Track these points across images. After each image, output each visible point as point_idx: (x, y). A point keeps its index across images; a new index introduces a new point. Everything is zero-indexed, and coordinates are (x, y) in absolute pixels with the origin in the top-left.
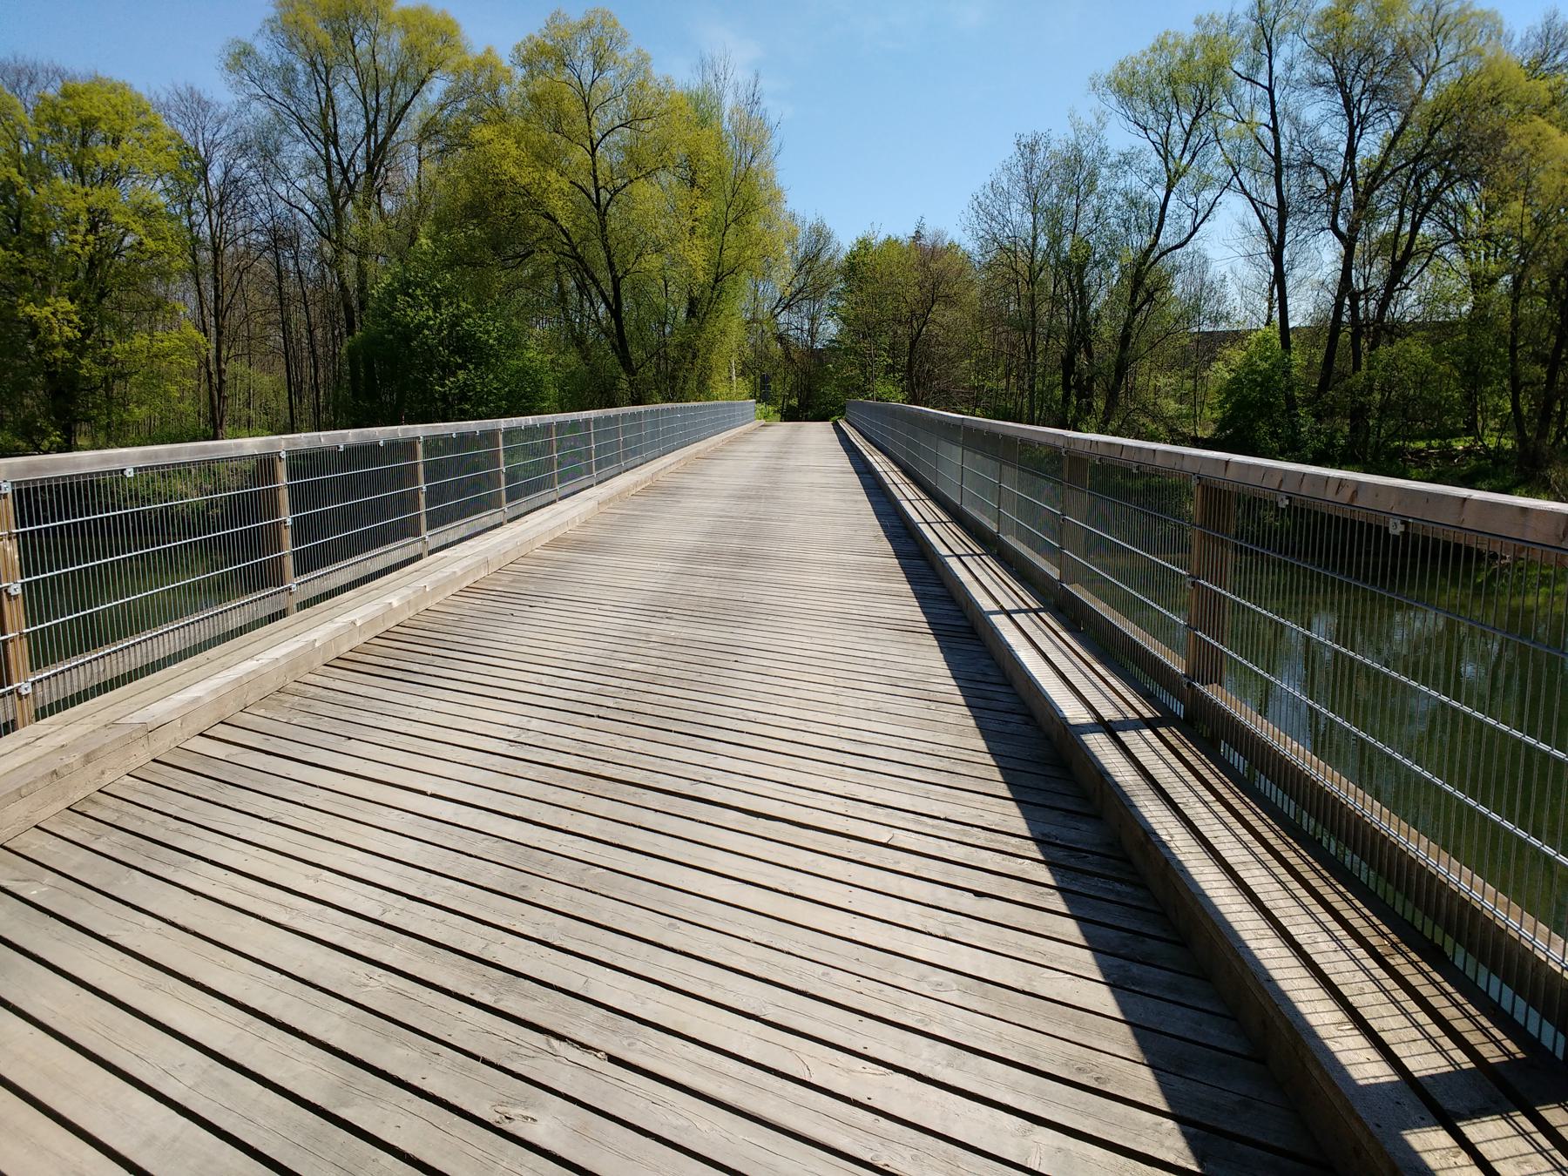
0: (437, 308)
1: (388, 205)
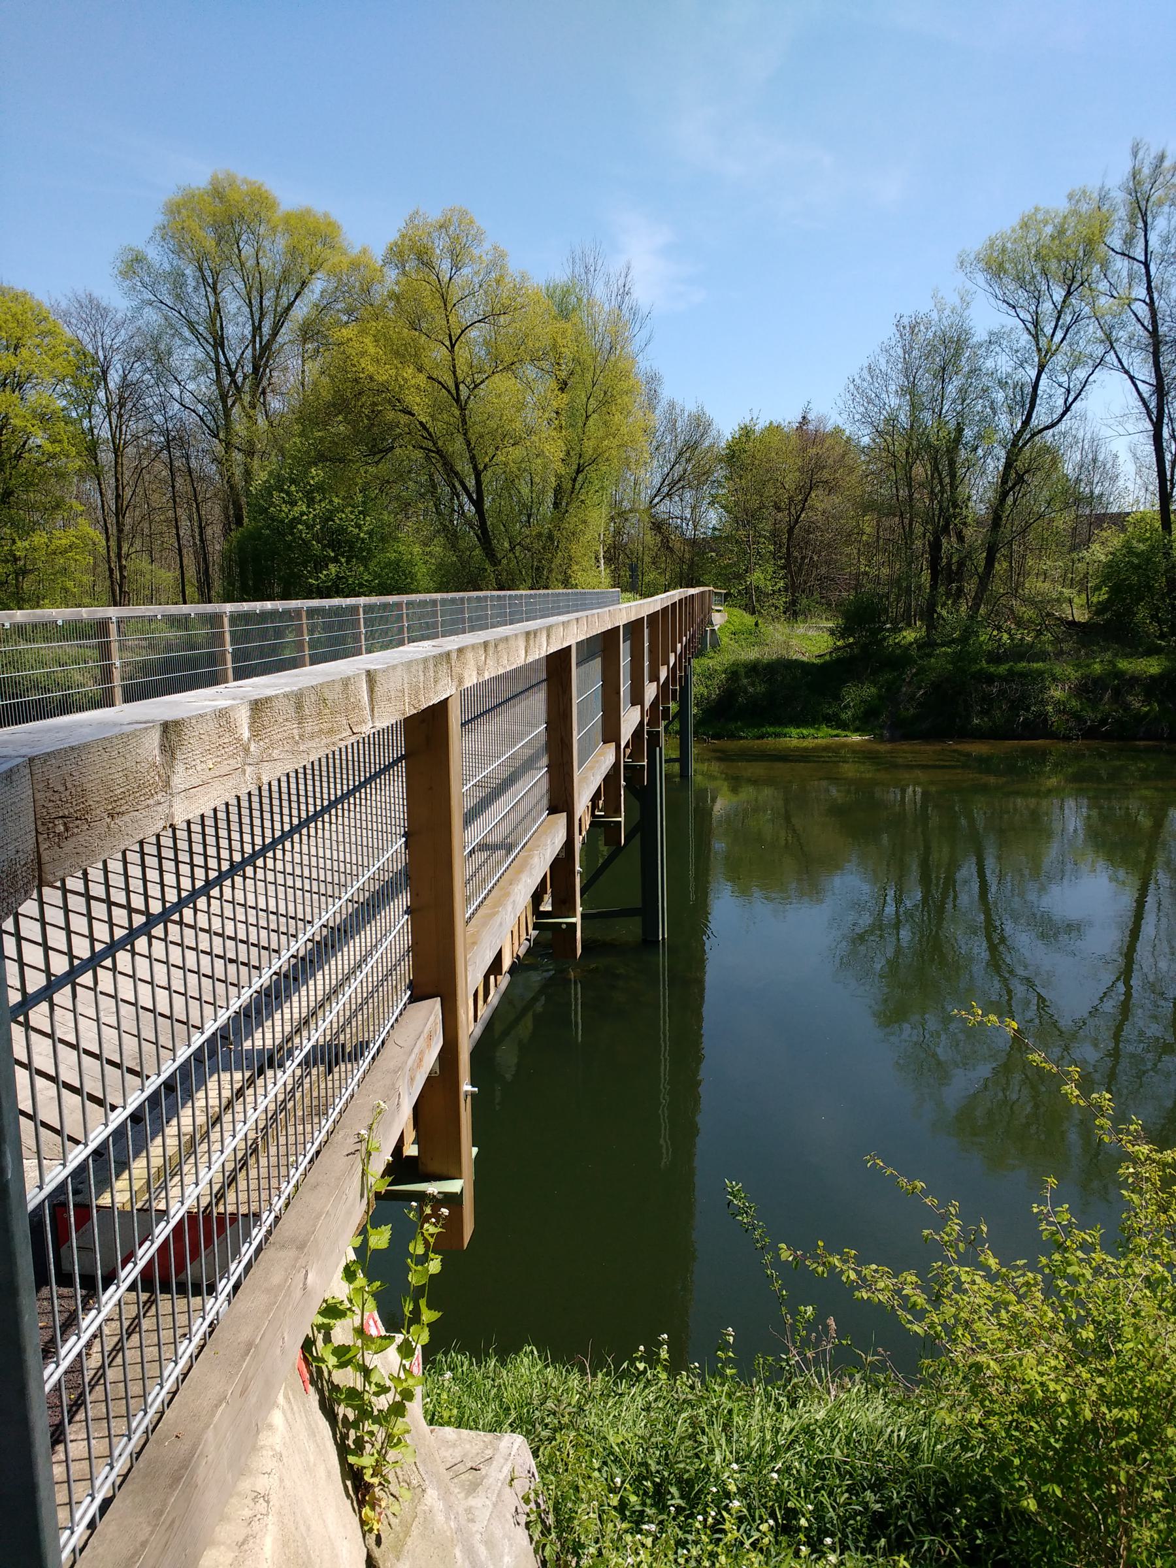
0: (311, 502)
1: (275, 404)
